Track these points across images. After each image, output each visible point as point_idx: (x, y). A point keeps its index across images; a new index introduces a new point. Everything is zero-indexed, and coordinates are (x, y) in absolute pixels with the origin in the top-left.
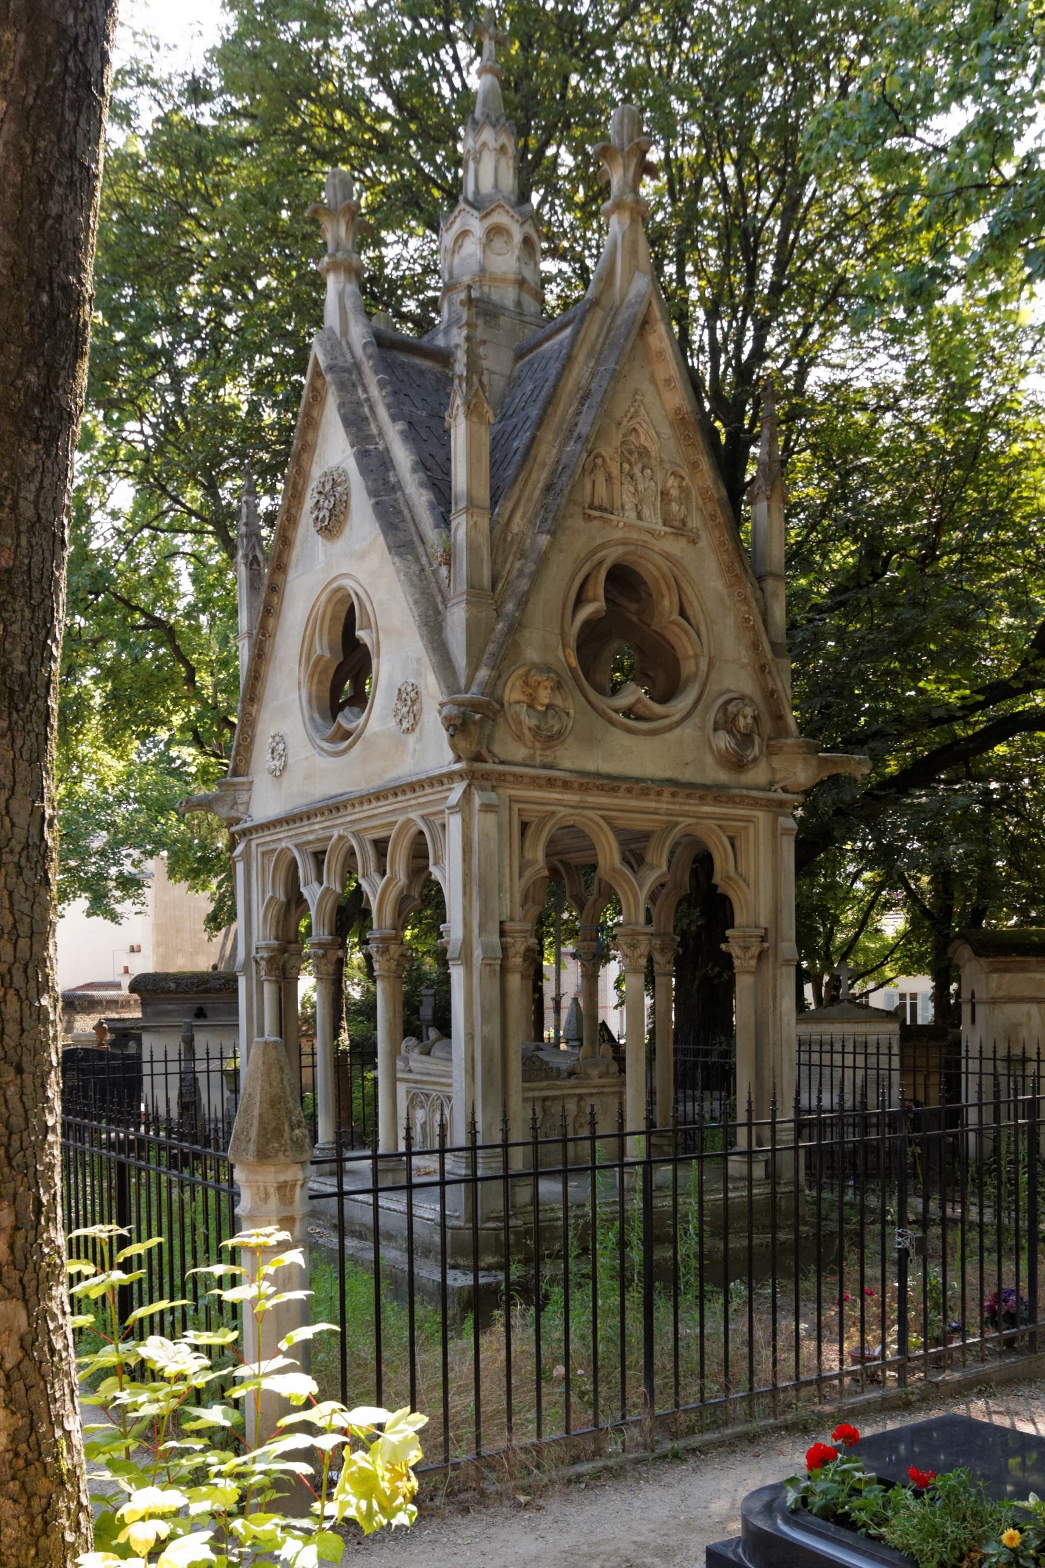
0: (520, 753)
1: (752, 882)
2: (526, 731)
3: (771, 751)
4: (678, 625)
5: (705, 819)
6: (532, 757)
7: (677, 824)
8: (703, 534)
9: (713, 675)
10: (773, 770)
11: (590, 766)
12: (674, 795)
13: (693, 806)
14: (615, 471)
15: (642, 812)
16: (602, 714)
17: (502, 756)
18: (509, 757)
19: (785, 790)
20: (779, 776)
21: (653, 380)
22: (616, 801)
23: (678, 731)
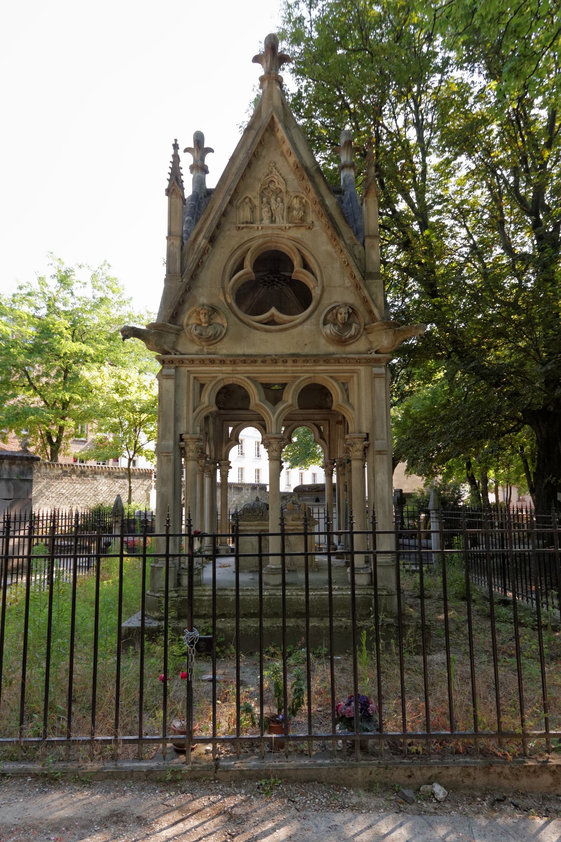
0: (195, 348)
1: (356, 406)
2: (194, 337)
3: (367, 331)
4: (301, 272)
5: (321, 374)
6: (202, 350)
7: (299, 377)
8: (316, 223)
9: (325, 295)
10: (371, 342)
11: (240, 351)
12: (294, 361)
13: (309, 367)
14: (257, 202)
15: (273, 374)
16: (248, 325)
17: (183, 352)
18: (188, 351)
19: (377, 352)
20: (374, 345)
21: (282, 154)
22: (256, 368)
23: (299, 328)
